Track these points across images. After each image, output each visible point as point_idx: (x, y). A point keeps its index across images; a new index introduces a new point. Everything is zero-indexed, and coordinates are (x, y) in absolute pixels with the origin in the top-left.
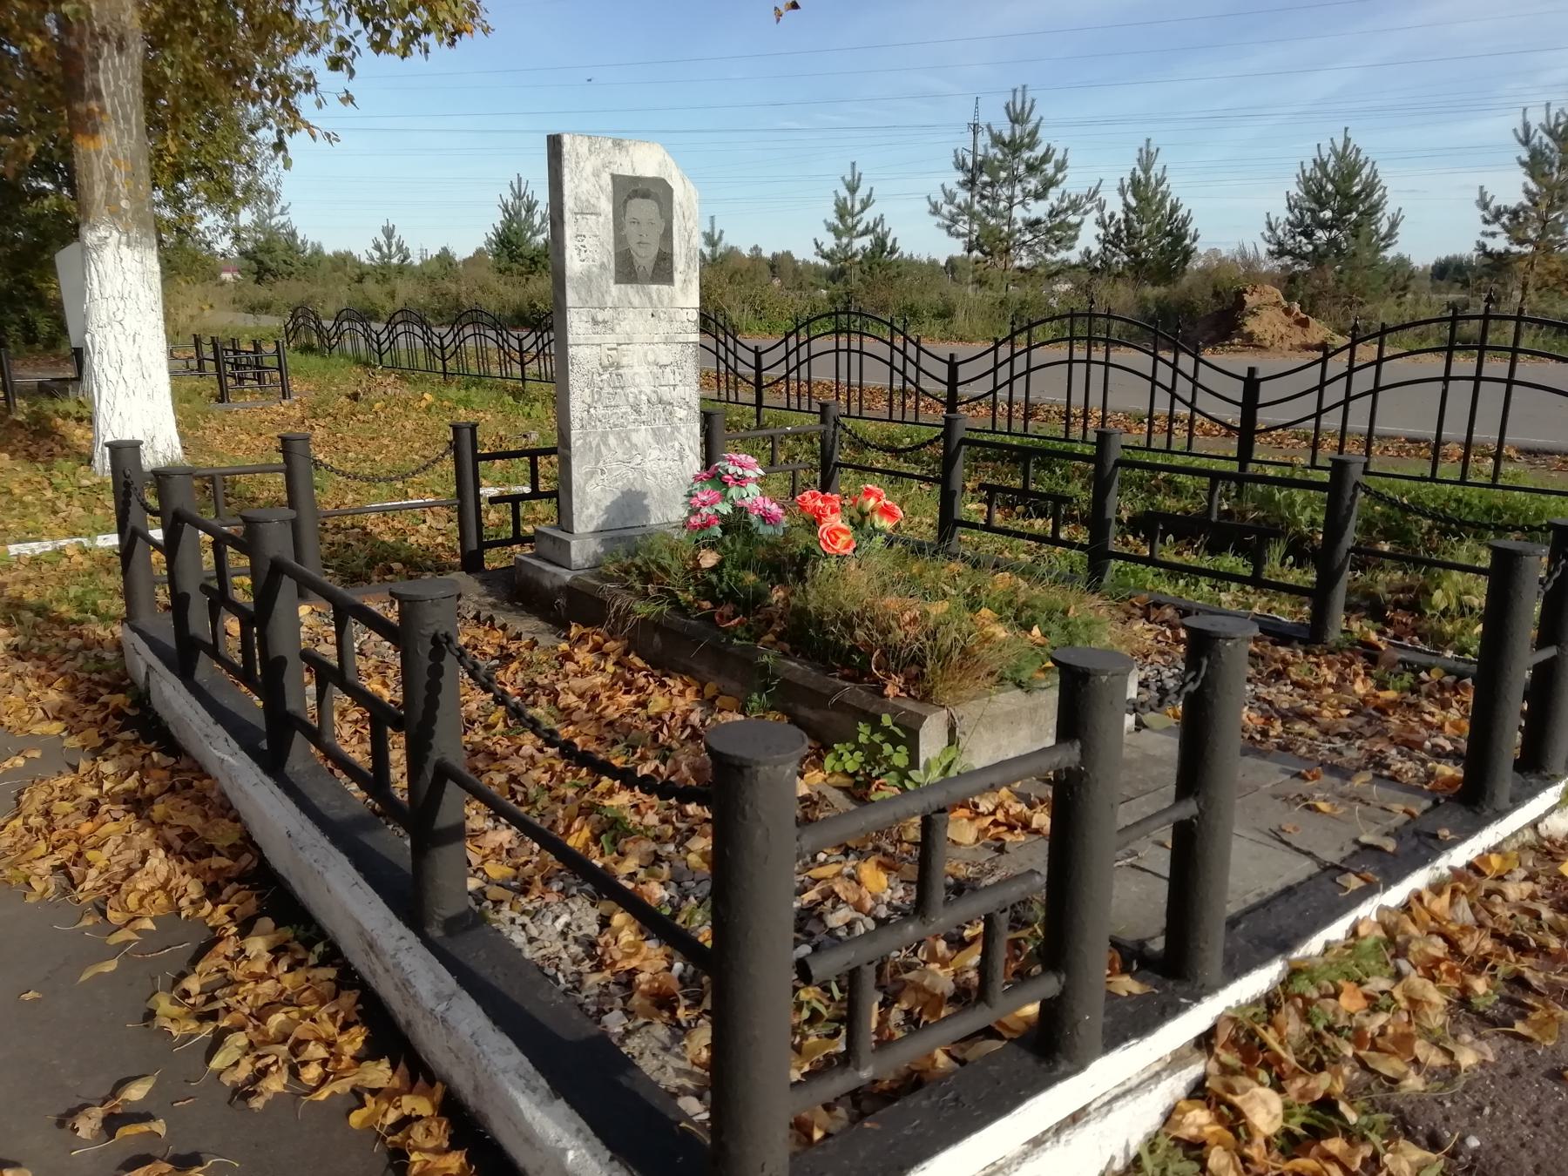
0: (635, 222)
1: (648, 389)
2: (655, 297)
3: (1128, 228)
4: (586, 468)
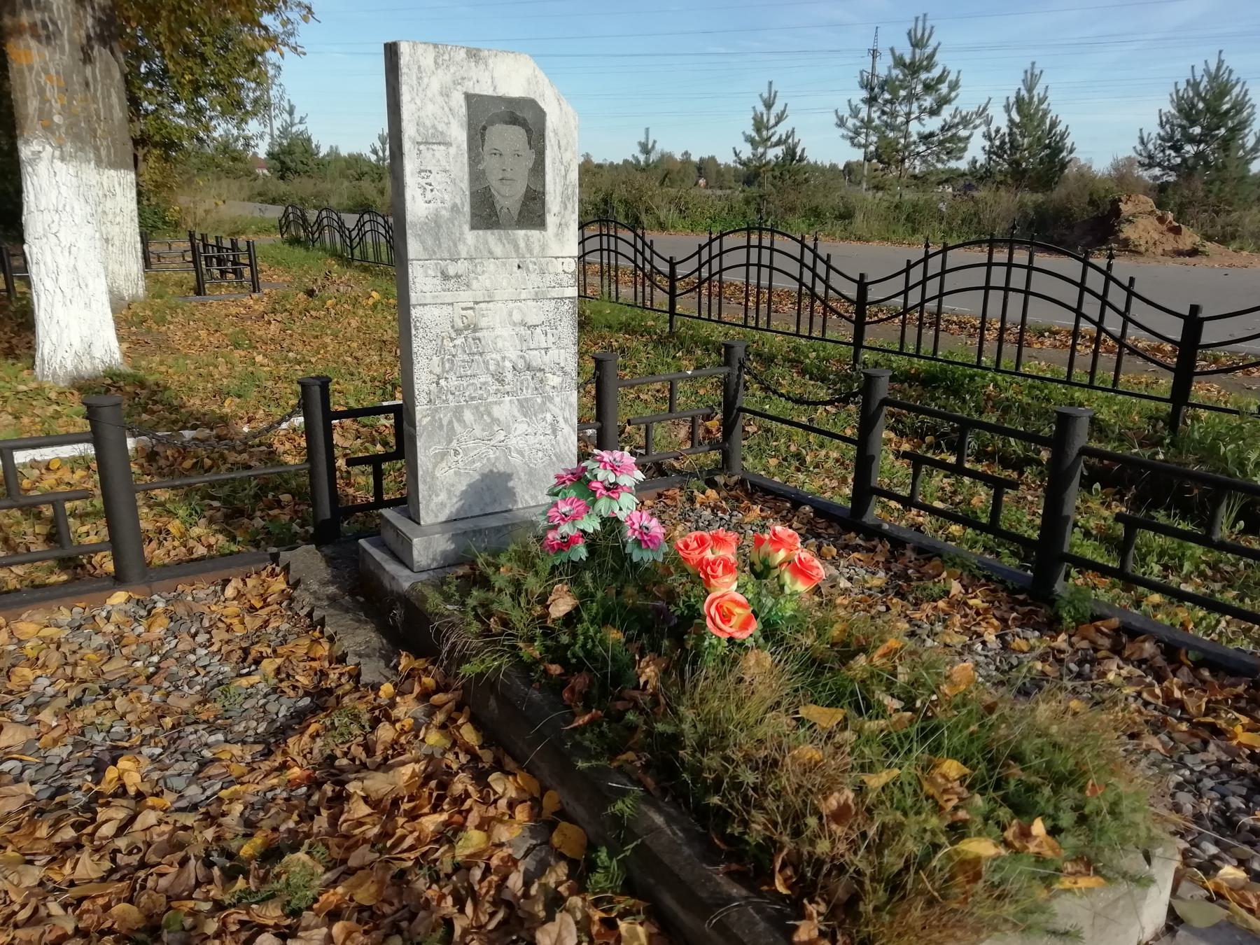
0: (497, 153)
1: (513, 354)
2: (522, 244)
3: (1012, 142)
4: (437, 448)
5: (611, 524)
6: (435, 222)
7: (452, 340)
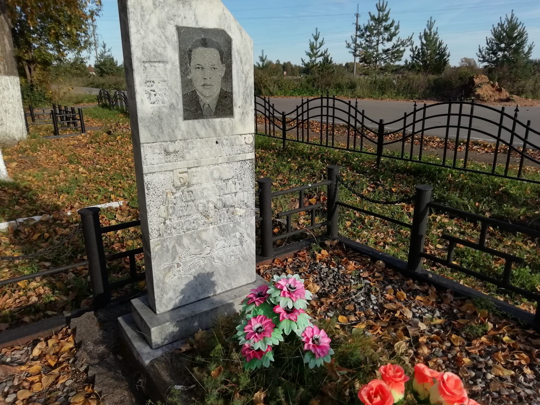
0: (200, 67)
1: (214, 199)
2: (218, 128)
3: (423, 52)
5: (291, 338)
6: (159, 116)
7: (173, 194)
